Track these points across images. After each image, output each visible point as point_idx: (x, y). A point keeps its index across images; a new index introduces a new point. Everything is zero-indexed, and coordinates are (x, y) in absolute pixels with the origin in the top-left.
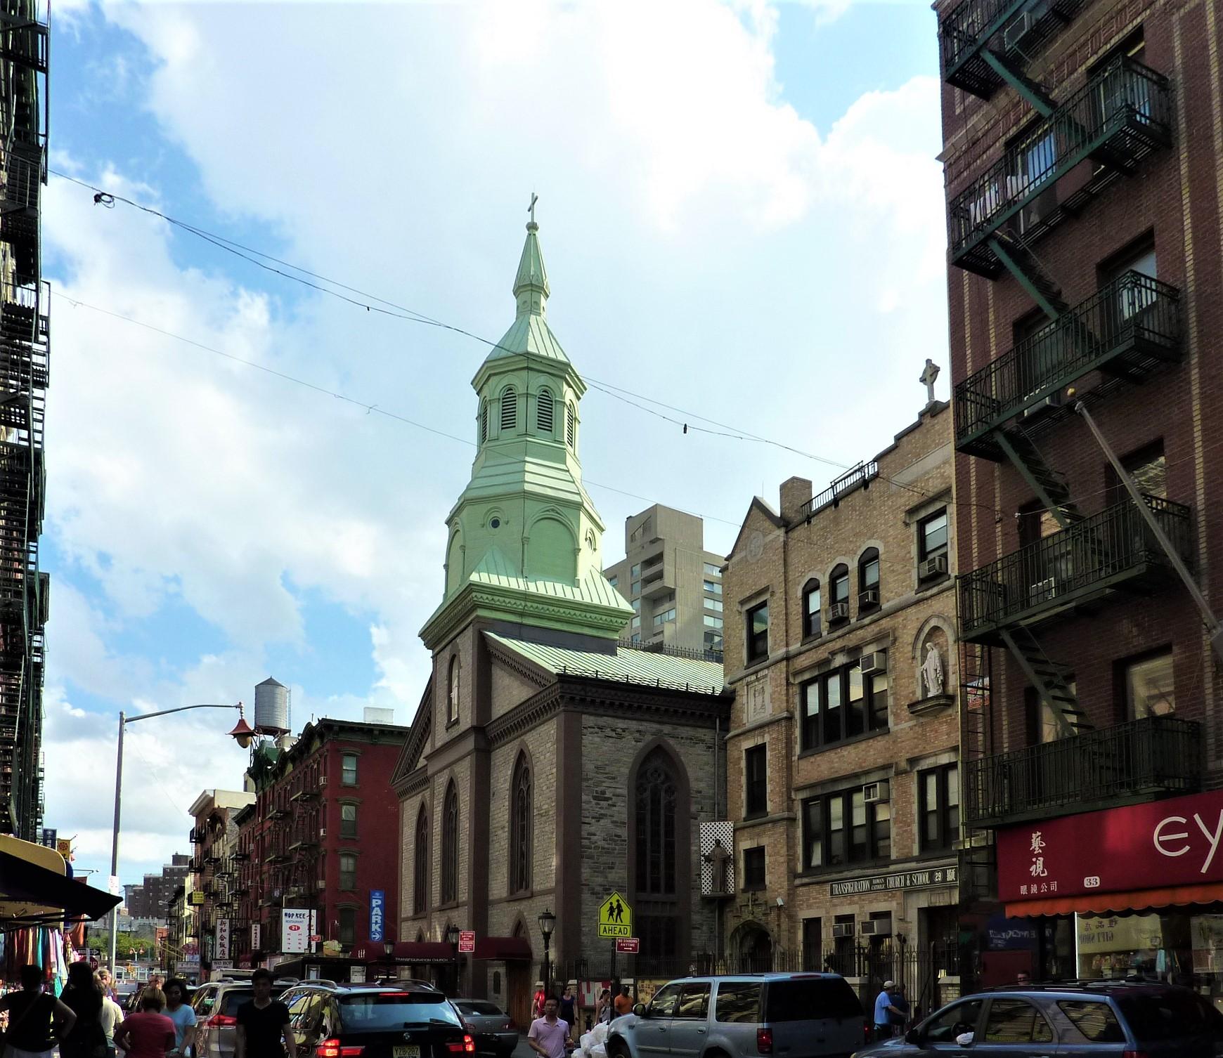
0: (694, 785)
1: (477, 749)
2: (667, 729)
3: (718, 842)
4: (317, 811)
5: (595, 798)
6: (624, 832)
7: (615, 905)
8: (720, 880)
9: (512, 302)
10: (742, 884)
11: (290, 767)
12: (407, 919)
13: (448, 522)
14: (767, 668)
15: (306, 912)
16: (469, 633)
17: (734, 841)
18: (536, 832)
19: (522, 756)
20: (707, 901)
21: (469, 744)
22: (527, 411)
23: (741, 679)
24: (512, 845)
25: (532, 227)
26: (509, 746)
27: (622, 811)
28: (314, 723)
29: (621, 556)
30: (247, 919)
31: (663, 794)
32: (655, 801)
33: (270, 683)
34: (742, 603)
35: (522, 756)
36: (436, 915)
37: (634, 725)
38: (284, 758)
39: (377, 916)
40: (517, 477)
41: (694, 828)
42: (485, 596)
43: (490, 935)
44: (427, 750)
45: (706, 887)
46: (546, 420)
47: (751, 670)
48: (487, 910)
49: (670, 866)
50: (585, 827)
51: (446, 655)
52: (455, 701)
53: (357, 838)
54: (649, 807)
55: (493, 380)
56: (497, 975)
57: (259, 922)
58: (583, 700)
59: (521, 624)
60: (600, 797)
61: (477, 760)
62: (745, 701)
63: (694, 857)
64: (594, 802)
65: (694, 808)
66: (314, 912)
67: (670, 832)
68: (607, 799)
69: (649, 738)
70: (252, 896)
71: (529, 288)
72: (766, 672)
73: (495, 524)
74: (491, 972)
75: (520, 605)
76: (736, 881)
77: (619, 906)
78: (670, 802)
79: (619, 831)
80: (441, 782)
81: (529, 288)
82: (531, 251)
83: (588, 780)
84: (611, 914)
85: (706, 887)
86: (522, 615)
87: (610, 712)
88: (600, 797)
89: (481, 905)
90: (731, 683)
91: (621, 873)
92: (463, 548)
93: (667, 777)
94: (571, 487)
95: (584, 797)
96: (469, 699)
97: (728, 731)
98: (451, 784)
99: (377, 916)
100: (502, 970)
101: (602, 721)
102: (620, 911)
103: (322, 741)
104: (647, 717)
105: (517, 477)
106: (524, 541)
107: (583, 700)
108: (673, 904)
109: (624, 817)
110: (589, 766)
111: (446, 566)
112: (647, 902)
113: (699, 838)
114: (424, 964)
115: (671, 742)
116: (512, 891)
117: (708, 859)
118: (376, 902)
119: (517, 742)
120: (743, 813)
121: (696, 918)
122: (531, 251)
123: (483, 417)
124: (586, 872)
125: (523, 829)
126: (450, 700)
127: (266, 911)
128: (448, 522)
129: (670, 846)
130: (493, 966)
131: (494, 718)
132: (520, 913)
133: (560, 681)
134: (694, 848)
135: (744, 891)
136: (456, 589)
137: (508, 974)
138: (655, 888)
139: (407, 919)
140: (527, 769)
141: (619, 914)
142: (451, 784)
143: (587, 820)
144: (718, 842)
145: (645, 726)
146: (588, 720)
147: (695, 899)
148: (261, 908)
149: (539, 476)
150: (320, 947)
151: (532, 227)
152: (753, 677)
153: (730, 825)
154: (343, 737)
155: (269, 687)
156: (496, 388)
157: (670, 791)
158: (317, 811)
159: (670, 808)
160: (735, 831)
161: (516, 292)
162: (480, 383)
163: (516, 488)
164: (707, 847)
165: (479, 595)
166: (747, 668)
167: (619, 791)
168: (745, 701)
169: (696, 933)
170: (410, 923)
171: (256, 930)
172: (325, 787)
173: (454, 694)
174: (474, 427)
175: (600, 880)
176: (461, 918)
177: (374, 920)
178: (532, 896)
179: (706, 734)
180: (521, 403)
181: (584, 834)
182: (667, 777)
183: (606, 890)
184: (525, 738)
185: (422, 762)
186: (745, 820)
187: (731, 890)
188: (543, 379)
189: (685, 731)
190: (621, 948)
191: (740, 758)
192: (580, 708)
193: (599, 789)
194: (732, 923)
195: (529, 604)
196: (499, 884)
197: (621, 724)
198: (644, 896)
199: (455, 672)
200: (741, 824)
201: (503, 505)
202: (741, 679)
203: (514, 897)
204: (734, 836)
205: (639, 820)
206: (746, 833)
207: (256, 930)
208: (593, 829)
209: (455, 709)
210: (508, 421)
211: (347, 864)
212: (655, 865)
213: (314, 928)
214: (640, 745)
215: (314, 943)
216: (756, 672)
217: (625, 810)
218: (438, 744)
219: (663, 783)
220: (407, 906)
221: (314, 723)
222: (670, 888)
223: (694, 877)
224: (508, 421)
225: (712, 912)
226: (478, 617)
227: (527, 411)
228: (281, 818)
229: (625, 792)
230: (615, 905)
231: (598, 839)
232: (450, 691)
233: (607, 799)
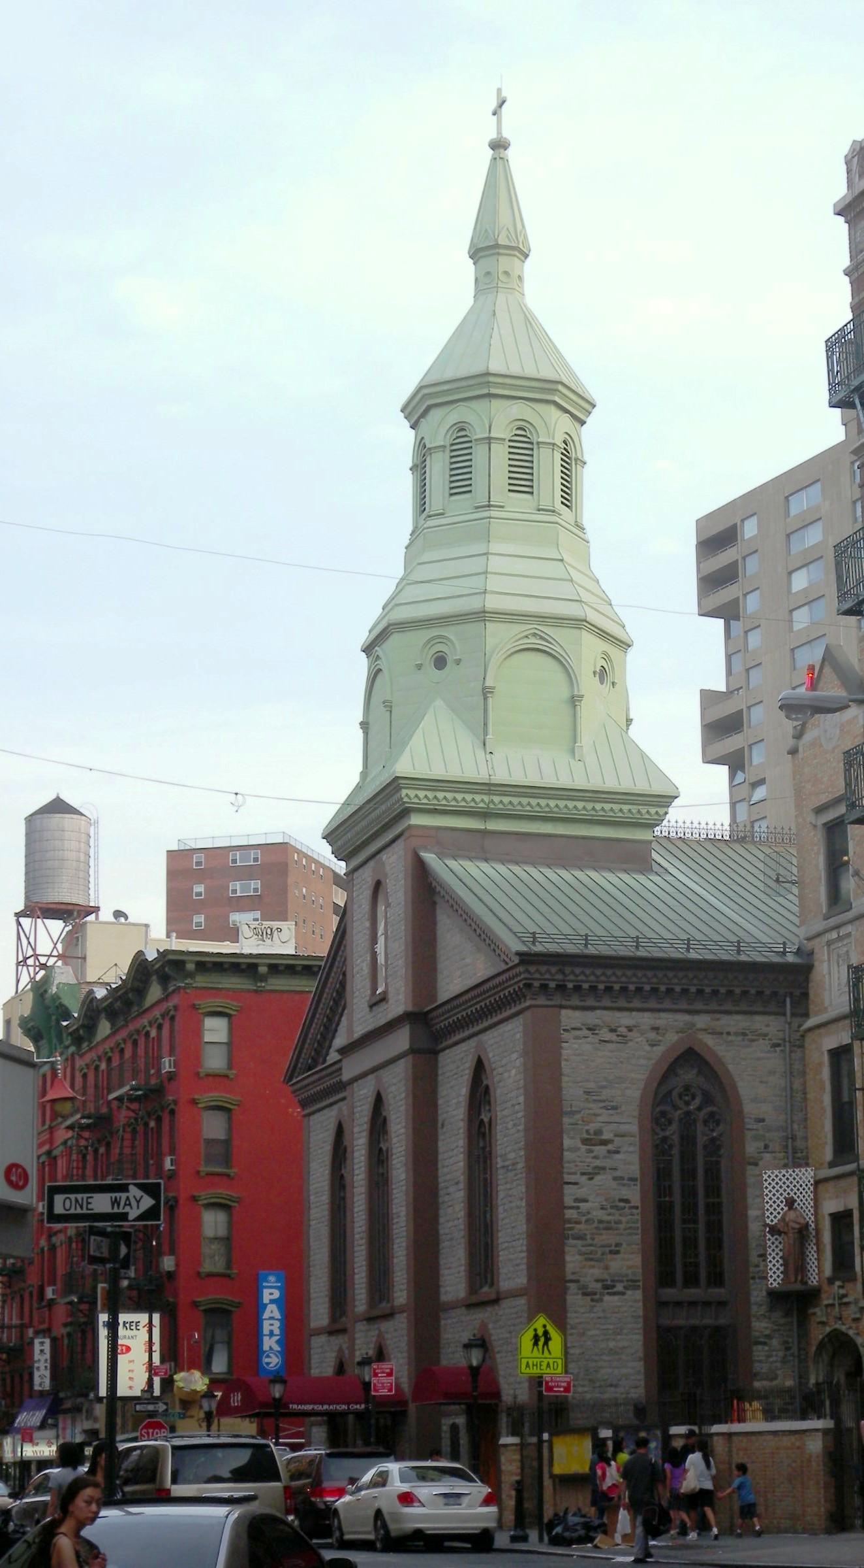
0: (749, 1108)
1: (413, 1051)
2: (702, 1021)
3: (790, 1203)
4: (159, 1120)
5: (585, 1142)
6: (634, 1194)
7: (540, 1332)
8: (796, 1264)
9: (468, 269)
10: (828, 1271)
11: (104, 1028)
12: (319, 1332)
13: (368, 649)
14: (851, 922)
15: (143, 1318)
16: (399, 846)
17: (816, 1200)
18: (501, 1195)
19: (480, 1067)
20: (776, 1297)
21: (401, 1040)
22: (495, 465)
23: (819, 935)
24: (470, 1215)
25: (499, 145)
26: (463, 1047)
27: (630, 1160)
28: (151, 956)
29: (843, 438)
30: (22, 1328)
31: (700, 1127)
32: (688, 1140)
33: (58, 806)
34: (819, 810)
35: (480, 1067)
36: (361, 1326)
37: (646, 1019)
38: (93, 1010)
39: (271, 1321)
40: (476, 565)
41: (751, 1180)
42: (421, 794)
43: (444, 1362)
44: (340, 1041)
45: (775, 1276)
46: (522, 480)
47: (832, 922)
48: (437, 1320)
49: (716, 1243)
50: (568, 1190)
51: (366, 876)
52: (381, 959)
53: (232, 1172)
54: (675, 1151)
55: (436, 415)
56: (454, 1428)
57: (46, 1332)
58: (561, 988)
59: (485, 833)
60: (593, 1140)
61: (414, 1066)
62: (825, 971)
63: (754, 1228)
64: (584, 1148)
65: (751, 1148)
66: (156, 1317)
67: (714, 1189)
68: (604, 1143)
69: (672, 1037)
70: (33, 1280)
71: (496, 250)
72: (849, 928)
73: (440, 662)
74: (446, 1424)
75: (481, 801)
76: (819, 1266)
77: (546, 1333)
78: (713, 1140)
79: (625, 1193)
80: (363, 1094)
81: (496, 250)
82: (498, 186)
83: (573, 1113)
84: (536, 1343)
85: (775, 1276)
86: (485, 815)
87: (606, 1002)
88: (593, 1140)
89: (428, 1311)
90: (809, 939)
91: (631, 1261)
92: (388, 705)
93: (708, 1099)
94: (566, 590)
95: (567, 1142)
96: (401, 962)
97: (806, 1015)
98: (379, 1100)
99: (271, 1321)
100: (461, 1421)
101: (592, 1018)
102: (547, 1338)
103: (165, 989)
104: (667, 1004)
105: (476, 583)
106: (486, 692)
107: (561, 988)
108: (722, 1304)
109: (635, 1169)
110: (572, 1091)
111: (365, 725)
112: (678, 1304)
113: (761, 1196)
114: (343, 1414)
115: (710, 1041)
116: (473, 1289)
117: (774, 1230)
118: (270, 1293)
119: (473, 1042)
120: (828, 1154)
121: (760, 1326)
122: (498, 186)
123: (420, 468)
124: (573, 1260)
125: (485, 1186)
126: (374, 955)
127: (60, 1312)
128: (368, 649)
129: (714, 1209)
130: (448, 1415)
131: (440, 1002)
132: (484, 1326)
133: (522, 962)
134: (752, 1213)
135: (831, 1281)
136: (380, 780)
137: (470, 1426)
138: (691, 1280)
139: (319, 1332)
140: (487, 1087)
141: (546, 1343)
142: (379, 1100)
143: (572, 1178)
144: (790, 1203)
145: (663, 1019)
146: (570, 1018)
147: (758, 1295)
148: (51, 1303)
149: (511, 573)
150: (168, 1383)
151: (499, 145)
152: (834, 935)
153: (807, 1175)
154: (201, 981)
155: (57, 819)
156: (440, 425)
157: (713, 1119)
158: (159, 1120)
159: (714, 1146)
160: (817, 1183)
161: (476, 254)
162: (418, 409)
163: (474, 604)
164: (774, 1212)
165: (412, 793)
166: (832, 1165)
167: (624, 1128)
168: (825, 971)
169: (759, 1352)
170: (323, 1339)
171: (42, 1351)
172: (171, 1077)
173: (380, 947)
174: (407, 482)
175: (597, 1272)
176: (397, 1334)
177: (266, 1327)
178: (496, 1301)
179: (771, 1025)
180: (479, 452)
181: (568, 1200)
182: (708, 1099)
183: (606, 1287)
184: (484, 1037)
185: (333, 1056)
186: (832, 1165)
187: (814, 1280)
188: (518, 410)
189: (734, 1022)
190: (549, 1389)
191: (821, 1064)
192: (557, 1000)
193: (592, 1127)
194: (818, 1334)
195: (496, 799)
196: (454, 1280)
197: (625, 1019)
198: (669, 1293)
199: (381, 908)
200: (826, 1172)
201: (449, 632)
202: (819, 935)
203: (376, 1313)
204: (815, 1192)
205: (660, 1176)
206: (830, 1186)
207: (42, 1351)
208: (581, 1192)
209: (382, 973)
210: (460, 482)
211: (213, 1223)
212: (690, 1242)
213: (156, 1347)
214: (659, 1050)
215: (157, 1381)
216: (837, 927)
217: (635, 1158)
218: (359, 1031)
219: (699, 1109)
220: (319, 1312)
221: (151, 956)
222: (717, 1278)
223: (754, 1258)
224: (460, 482)
225: (787, 1314)
226: (410, 827)
227: (495, 465)
228: (88, 1127)
229: (634, 1128)
230: (540, 1332)
231: (593, 1207)
232: (374, 940)
233: (604, 1143)
